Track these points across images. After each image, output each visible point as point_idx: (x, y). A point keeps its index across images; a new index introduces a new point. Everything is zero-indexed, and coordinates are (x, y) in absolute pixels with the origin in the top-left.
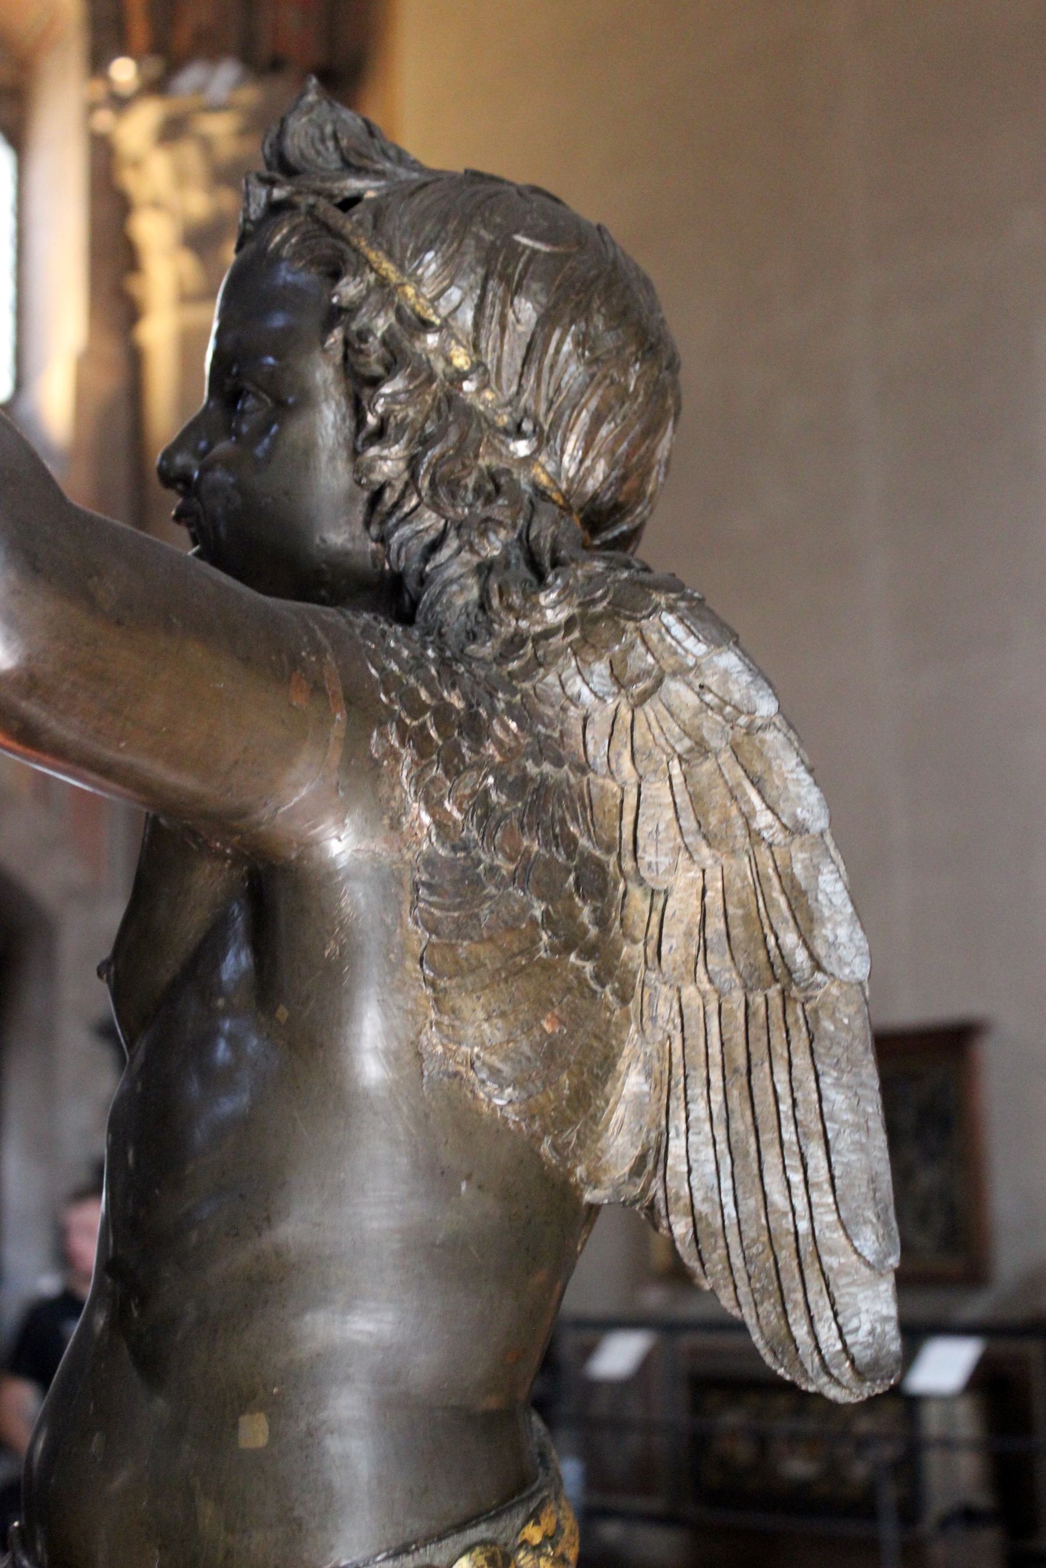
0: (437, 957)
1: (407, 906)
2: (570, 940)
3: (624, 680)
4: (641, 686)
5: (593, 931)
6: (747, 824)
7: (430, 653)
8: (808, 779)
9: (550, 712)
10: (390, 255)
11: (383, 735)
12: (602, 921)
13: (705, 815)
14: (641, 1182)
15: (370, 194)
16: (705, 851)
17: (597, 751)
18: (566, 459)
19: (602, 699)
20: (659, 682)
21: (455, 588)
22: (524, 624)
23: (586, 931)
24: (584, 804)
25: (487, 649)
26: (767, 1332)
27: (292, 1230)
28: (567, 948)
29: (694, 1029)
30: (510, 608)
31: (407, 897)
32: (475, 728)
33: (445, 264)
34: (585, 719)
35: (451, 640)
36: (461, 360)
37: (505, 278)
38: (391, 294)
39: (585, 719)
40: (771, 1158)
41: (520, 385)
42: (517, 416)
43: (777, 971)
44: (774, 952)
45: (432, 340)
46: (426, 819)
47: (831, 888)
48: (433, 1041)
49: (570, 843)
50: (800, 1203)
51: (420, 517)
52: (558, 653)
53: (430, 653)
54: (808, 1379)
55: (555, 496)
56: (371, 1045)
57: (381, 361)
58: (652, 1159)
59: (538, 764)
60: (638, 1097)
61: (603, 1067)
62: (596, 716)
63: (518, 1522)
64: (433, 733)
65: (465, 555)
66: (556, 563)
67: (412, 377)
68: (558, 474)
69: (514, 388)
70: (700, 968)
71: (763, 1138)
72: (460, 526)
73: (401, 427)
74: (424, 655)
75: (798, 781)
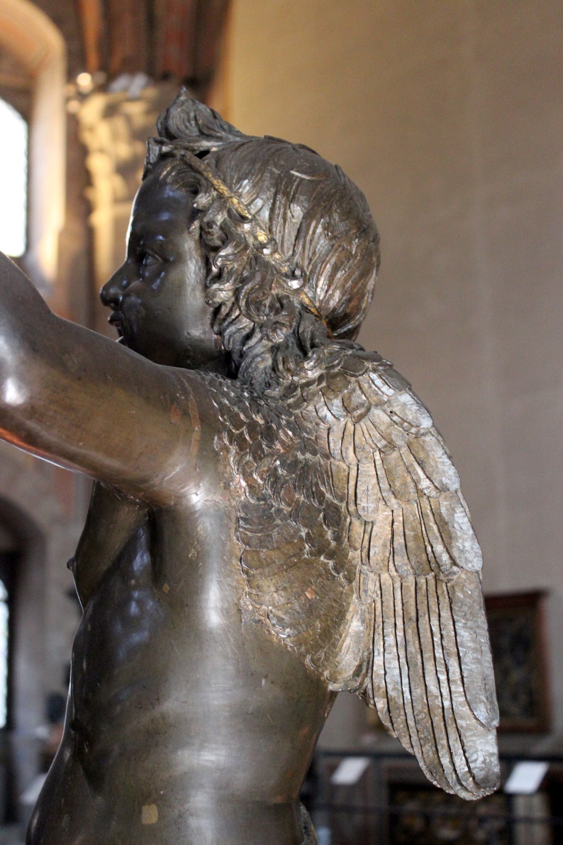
1: (233, 530)
2: (321, 549)
5: (333, 544)
6: (416, 486)
9: (310, 426)
10: (224, 181)
11: (220, 439)
12: (338, 538)
14: (359, 680)
15: (214, 149)
16: (393, 501)
17: (335, 446)
18: (319, 290)
20: (368, 410)
21: (259, 359)
22: (296, 378)
23: (329, 544)
24: (328, 475)
25: (276, 392)
28: (319, 553)
29: (388, 597)
30: (288, 370)
31: (233, 525)
32: (270, 435)
34: (329, 429)
35: (257, 387)
36: (262, 237)
39: (329, 429)
40: (429, 666)
41: (294, 251)
42: (292, 267)
43: (432, 565)
44: (431, 555)
45: (247, 227)
46: (244, 484)
47: (461, 521)
48: (247, 603)
50: (445, 691)
52: (314, 395)
55: (313, 310)
56: (214, 605)
58: (365, 667)
59: (303, 454)
60: (358, 633)
61: (338, 618)
62: (335, 428)
64: (247, 437)
65: (265, 342)
66: (313, 346)
67: (236, 246)
68: (315, 298)
69: (291, 252)
70: (391, 564)
71: (425, 656)
73: (230, 273)
74: (242, 396)
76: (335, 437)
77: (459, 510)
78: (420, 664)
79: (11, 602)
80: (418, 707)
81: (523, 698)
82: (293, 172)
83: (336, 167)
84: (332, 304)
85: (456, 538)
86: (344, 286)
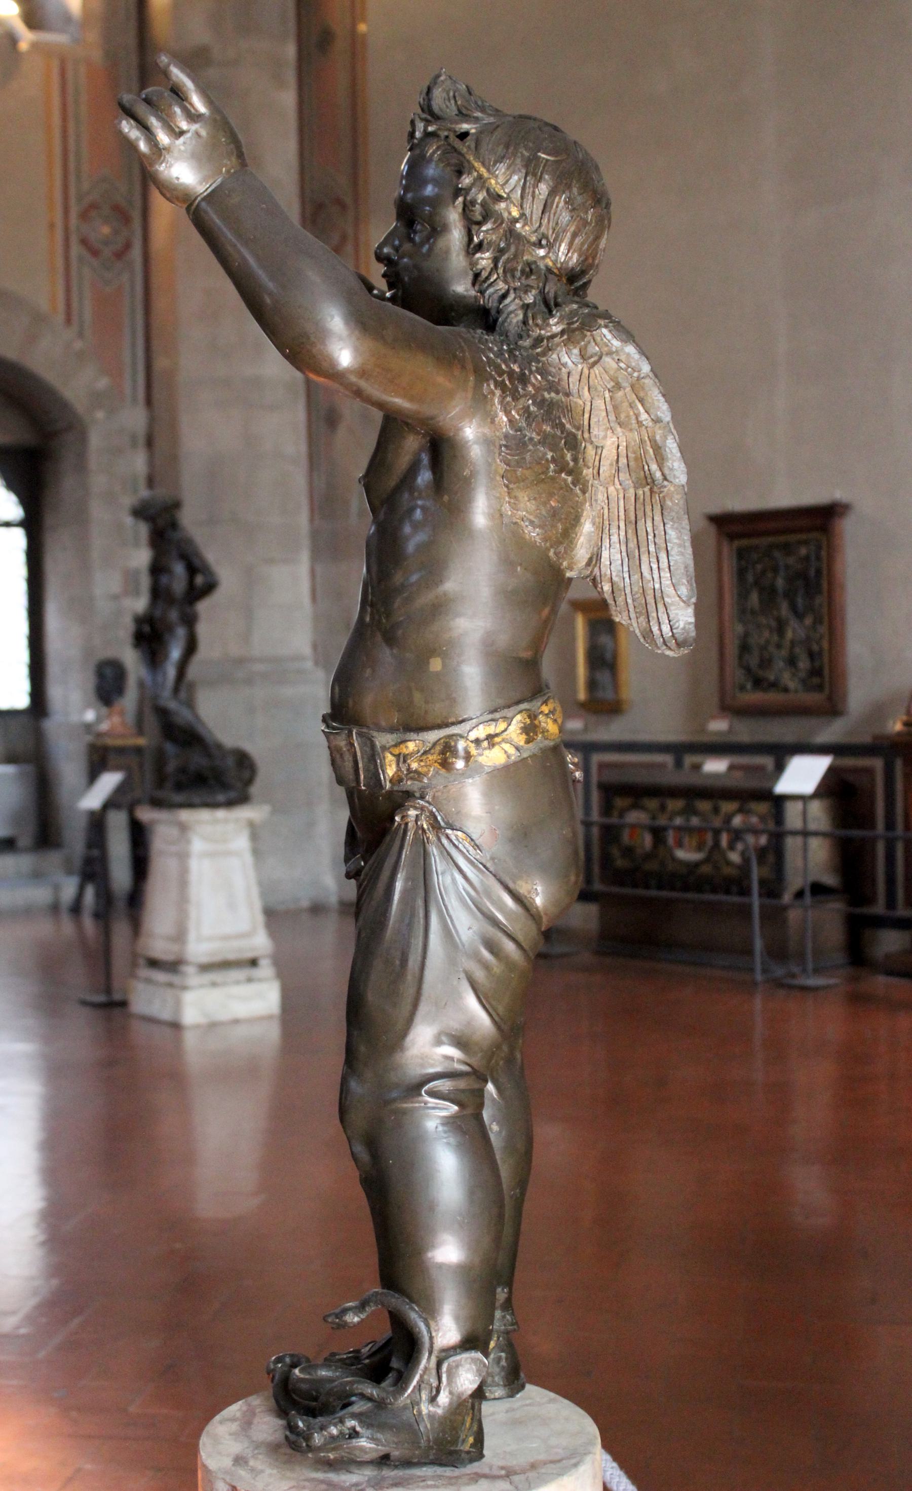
0: (509, 475)
1: (497, 455)
2: (563, 468)
3: (586, 357)
4: (592, 360)
5: (572, 464)
6: (637, 418)
7: (505, 347)
8: (662, 399)
9: (553, 370)
10: (483, 164)
11: (488, 385)
12: (575, 460)
13: (619, 414)
14: (590, 569)
15: (473, 131)
16: (619, 429)
17: (574, 388)
18: (560, 254)
19: (576, 365)
20: (600, 358)
21: (513, 315)
22: (543, 332)
23: (568, 464)
24: (568, 410)
25: (527, 343)
26: (642, 629)
27: (450, 586)
28: (561, 471)
29: (613, 505)
30: (537, 325)
31: (497, 451)
32: (523, 379)
33: (508, 169)
34: (569, 373)
35: (511, 338)
36: (515, 213)
37: (534, 175)
38: (484, 182)
39: (569, 373)
40: (644, 558)
41: (541, 223)
42: (540, 237)
43: (648, 480)
44: (647, 472)
45: (503, 205)
46: (505, 419)
47: (672, 446)
48: (507, 509)
49: (562, 426)
50: (656, 576)
51: (498, 284)
52: (558, 345)
53: (505, 347)
54: (658, 648)
55: (555, 271)
56: (481, 512)
57: (481, 214)
58: (595, 559)
59: (549, 393)
60: (589, 533)
61: (574, 521)
62: (574, 372)
63: (539, 704)
64: (507, 382)
65: (517, 301)
66: (557, 305)
67: (494, 223)
68: (556, 260)
69: (538, 224)
70: (616, 479)
71: (641, 550)
72: (515, 289)
73: (490, 244)
74: (502, 349)
75: (658, 400)
76: (574, 379)
77: (670, 437)
78: (637, 556)
79: (33, 525)
80: (635, 589)
81: (804, 664)
82: (539, 154)
83: (575, 142)
84: (571, 264)
85: (667, 459)
86: (581, 249)
